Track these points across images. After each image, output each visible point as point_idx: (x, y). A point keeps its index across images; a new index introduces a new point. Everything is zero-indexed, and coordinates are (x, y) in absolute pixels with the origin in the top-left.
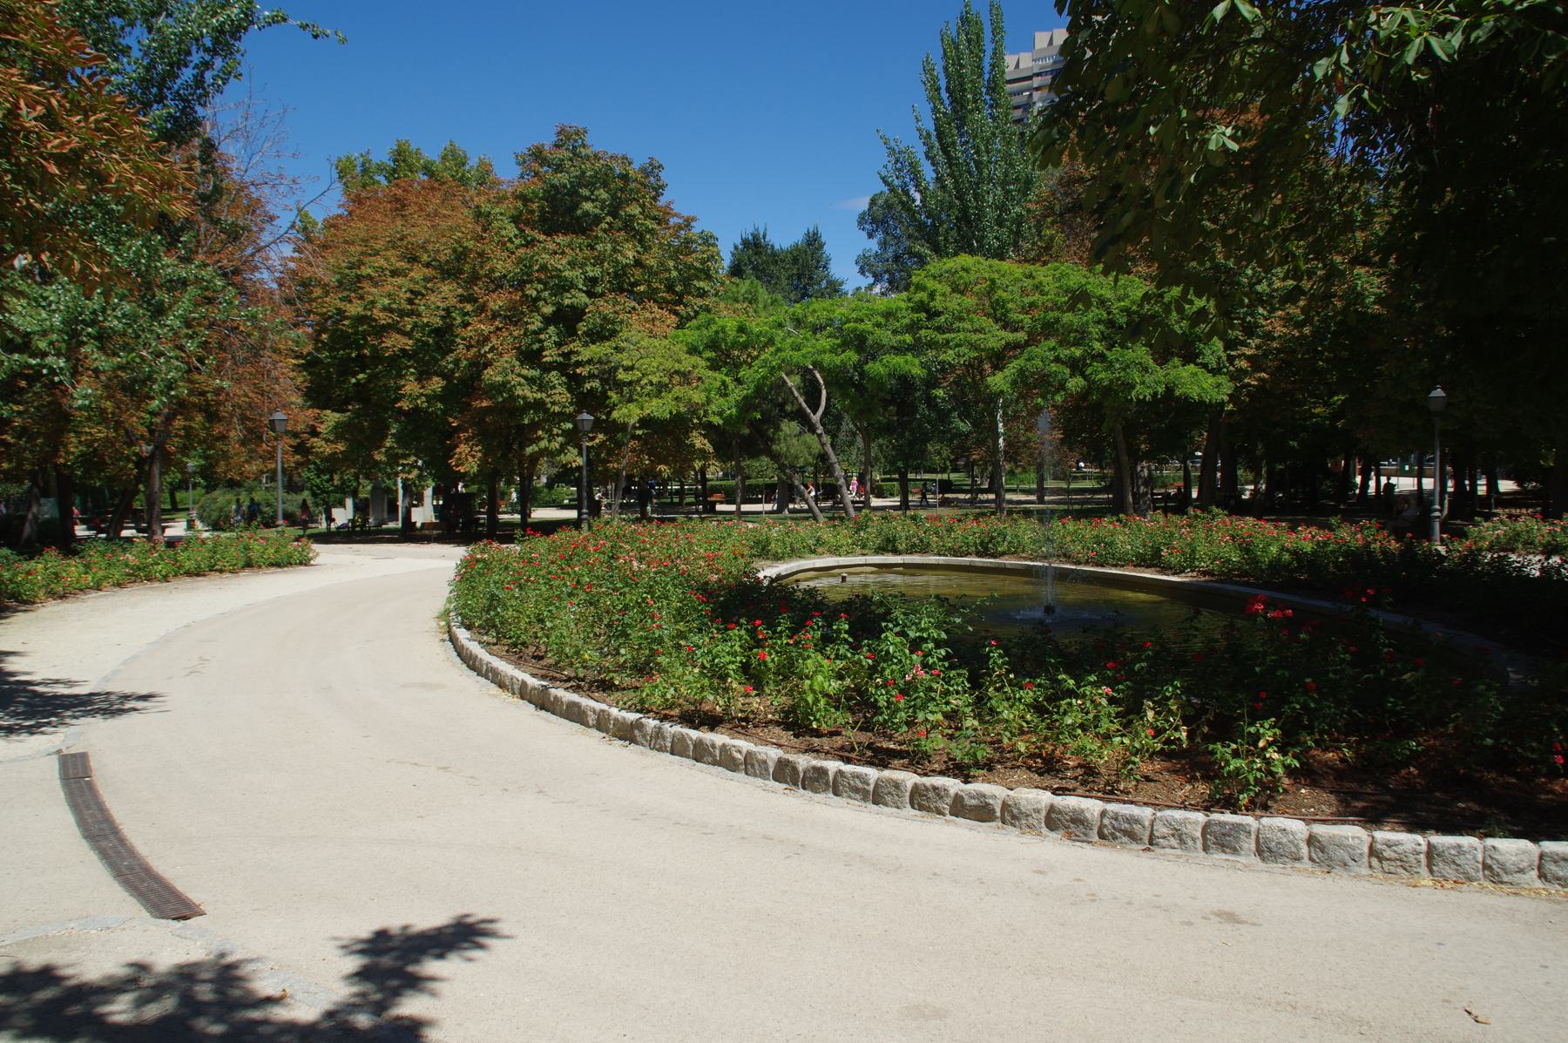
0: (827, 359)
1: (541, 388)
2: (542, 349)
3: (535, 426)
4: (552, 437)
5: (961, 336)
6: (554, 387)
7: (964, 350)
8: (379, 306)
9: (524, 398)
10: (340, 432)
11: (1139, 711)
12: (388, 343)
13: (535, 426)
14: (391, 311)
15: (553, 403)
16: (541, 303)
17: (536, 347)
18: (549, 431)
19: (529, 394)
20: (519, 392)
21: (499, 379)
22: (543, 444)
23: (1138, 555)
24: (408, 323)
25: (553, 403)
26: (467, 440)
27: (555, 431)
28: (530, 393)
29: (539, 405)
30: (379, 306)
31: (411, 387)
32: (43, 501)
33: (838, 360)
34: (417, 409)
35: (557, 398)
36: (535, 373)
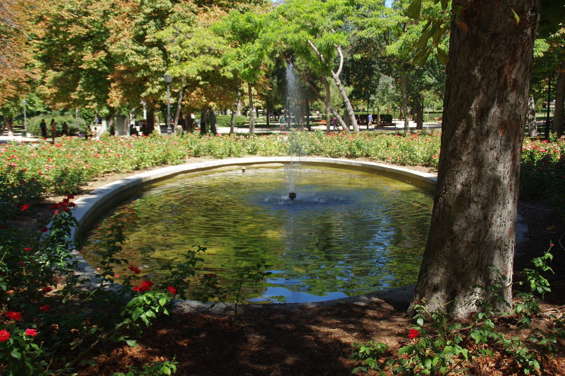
0: (290, 37)
1: (146, 56)
2: (145, 34)
3: (146, 79)
4: (153, 86)
5: (372, 19)
6: (154, 56)
7: (374, 28)
8: (66, 8)
9: (136, 63)
10: (56, 82)
11: (388, 301)
12: (72, 30)
13: (146, 79)
14: (72, 12)
15: (153, 66)
16: (144, 7)
17: (141, 32)
18: (152, 83)
19: (137, 60)
20: (131, 59)
21: (120, 51)
22: (149, 90)
23: (481, 173)
24: (85, 19)
25: (153, 66)
26: (115, 87)
27: (155, 82)
28: (140, 60)
29: (146, 67)
30: (66, 8)
31: (88, 56)
32: (109, 95)
33: (296, 37)
34: (91, 69)
35: (155, 62)
36: (140, 48)
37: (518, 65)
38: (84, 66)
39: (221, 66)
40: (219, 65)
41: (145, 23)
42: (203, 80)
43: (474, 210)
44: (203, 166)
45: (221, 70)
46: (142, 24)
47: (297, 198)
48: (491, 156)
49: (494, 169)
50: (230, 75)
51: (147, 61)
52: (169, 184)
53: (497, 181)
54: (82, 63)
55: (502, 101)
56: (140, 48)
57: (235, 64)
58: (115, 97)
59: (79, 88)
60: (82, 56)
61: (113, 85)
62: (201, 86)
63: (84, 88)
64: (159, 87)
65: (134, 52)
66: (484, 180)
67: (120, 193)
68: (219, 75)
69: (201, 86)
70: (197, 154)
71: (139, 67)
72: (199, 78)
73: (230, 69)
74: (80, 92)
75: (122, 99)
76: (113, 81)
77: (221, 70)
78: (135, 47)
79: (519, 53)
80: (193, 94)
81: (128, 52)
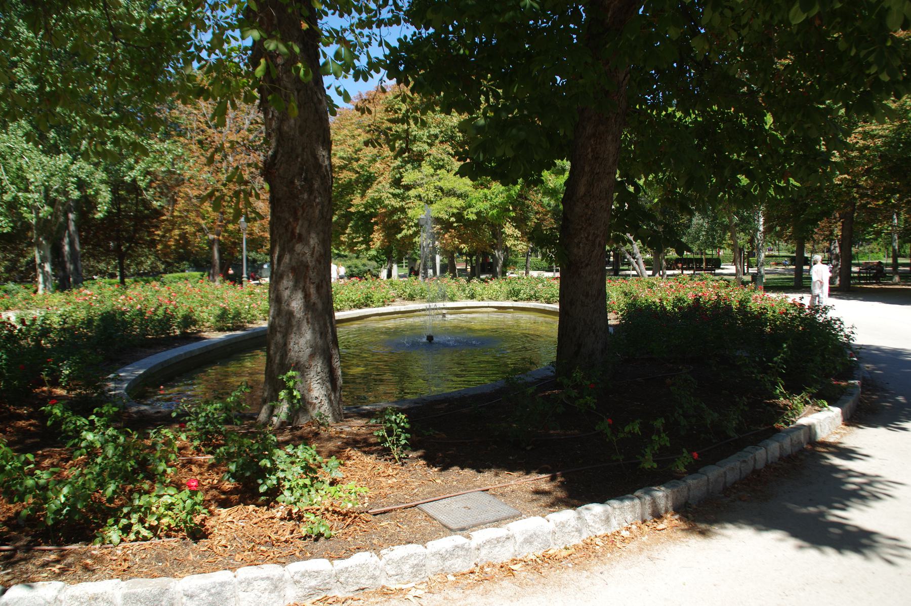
1: (403, 199)
2: (402, 177)
17: (398, 176)
19: (393, 203)
20: (387, 202)
22: (404, 232)
24: (355, 165)
26: (378, 230)
28: (396, 203)
34: (359, 212)
36: (397, 191)
37: (300, 222)
38: (353, 210)
39: (464, 209)
40: (463, 207)
41: (402, 167)
42: (456, 222)
43: (279, 337)
44: (403, 309)
45: (465, 213)
46: (399, 167)
47: (435, 339)
48: (286, 293)
49: (288, 305)
50: (473, 217)
51: (404, 203)
52: (355, 326)
53: (291, 314)
54: (351, 206)
55: (292, 251)
56: (397, 191)
57: (482, 206)
58: (378, 238)
59: (348, 231)
60: (351, 200)
61: (376, 227)
62: (455, 228)
63: (353, 230)
64: (414, 229)
65: (390, 196)
66: (284, 314)
67: (893, 354)
68: (463, 217)
69: (455, 228)
70: (411, 298)
71: (395, 210)
72: (453, 219)
73: (475, 210)
74: (349, 234)
75: (383, 241)
76: (376, 223)
77: (465, 213)
78: (391, 191)
79: (300, 213)
80: (446, 236)
81: (384, 195)
